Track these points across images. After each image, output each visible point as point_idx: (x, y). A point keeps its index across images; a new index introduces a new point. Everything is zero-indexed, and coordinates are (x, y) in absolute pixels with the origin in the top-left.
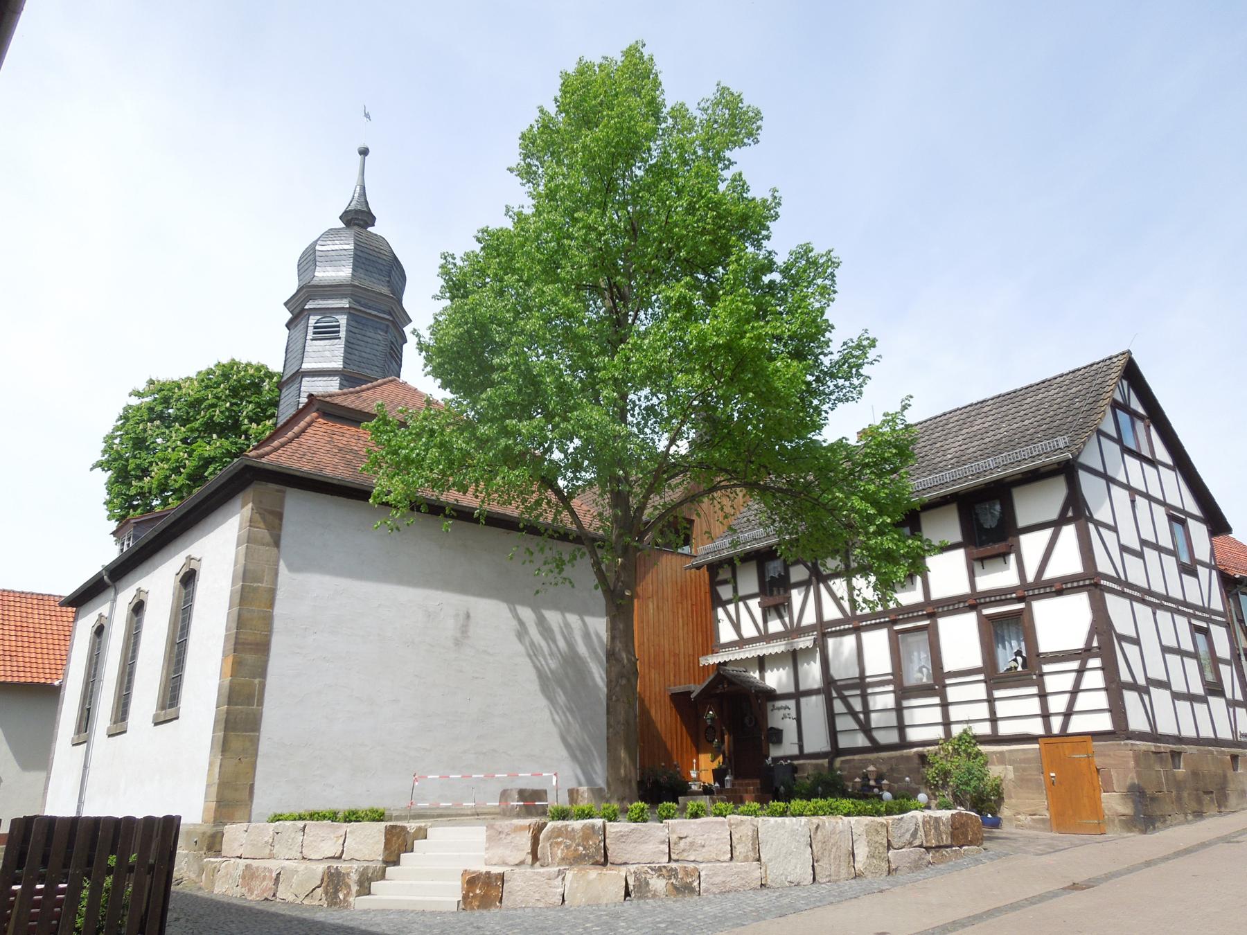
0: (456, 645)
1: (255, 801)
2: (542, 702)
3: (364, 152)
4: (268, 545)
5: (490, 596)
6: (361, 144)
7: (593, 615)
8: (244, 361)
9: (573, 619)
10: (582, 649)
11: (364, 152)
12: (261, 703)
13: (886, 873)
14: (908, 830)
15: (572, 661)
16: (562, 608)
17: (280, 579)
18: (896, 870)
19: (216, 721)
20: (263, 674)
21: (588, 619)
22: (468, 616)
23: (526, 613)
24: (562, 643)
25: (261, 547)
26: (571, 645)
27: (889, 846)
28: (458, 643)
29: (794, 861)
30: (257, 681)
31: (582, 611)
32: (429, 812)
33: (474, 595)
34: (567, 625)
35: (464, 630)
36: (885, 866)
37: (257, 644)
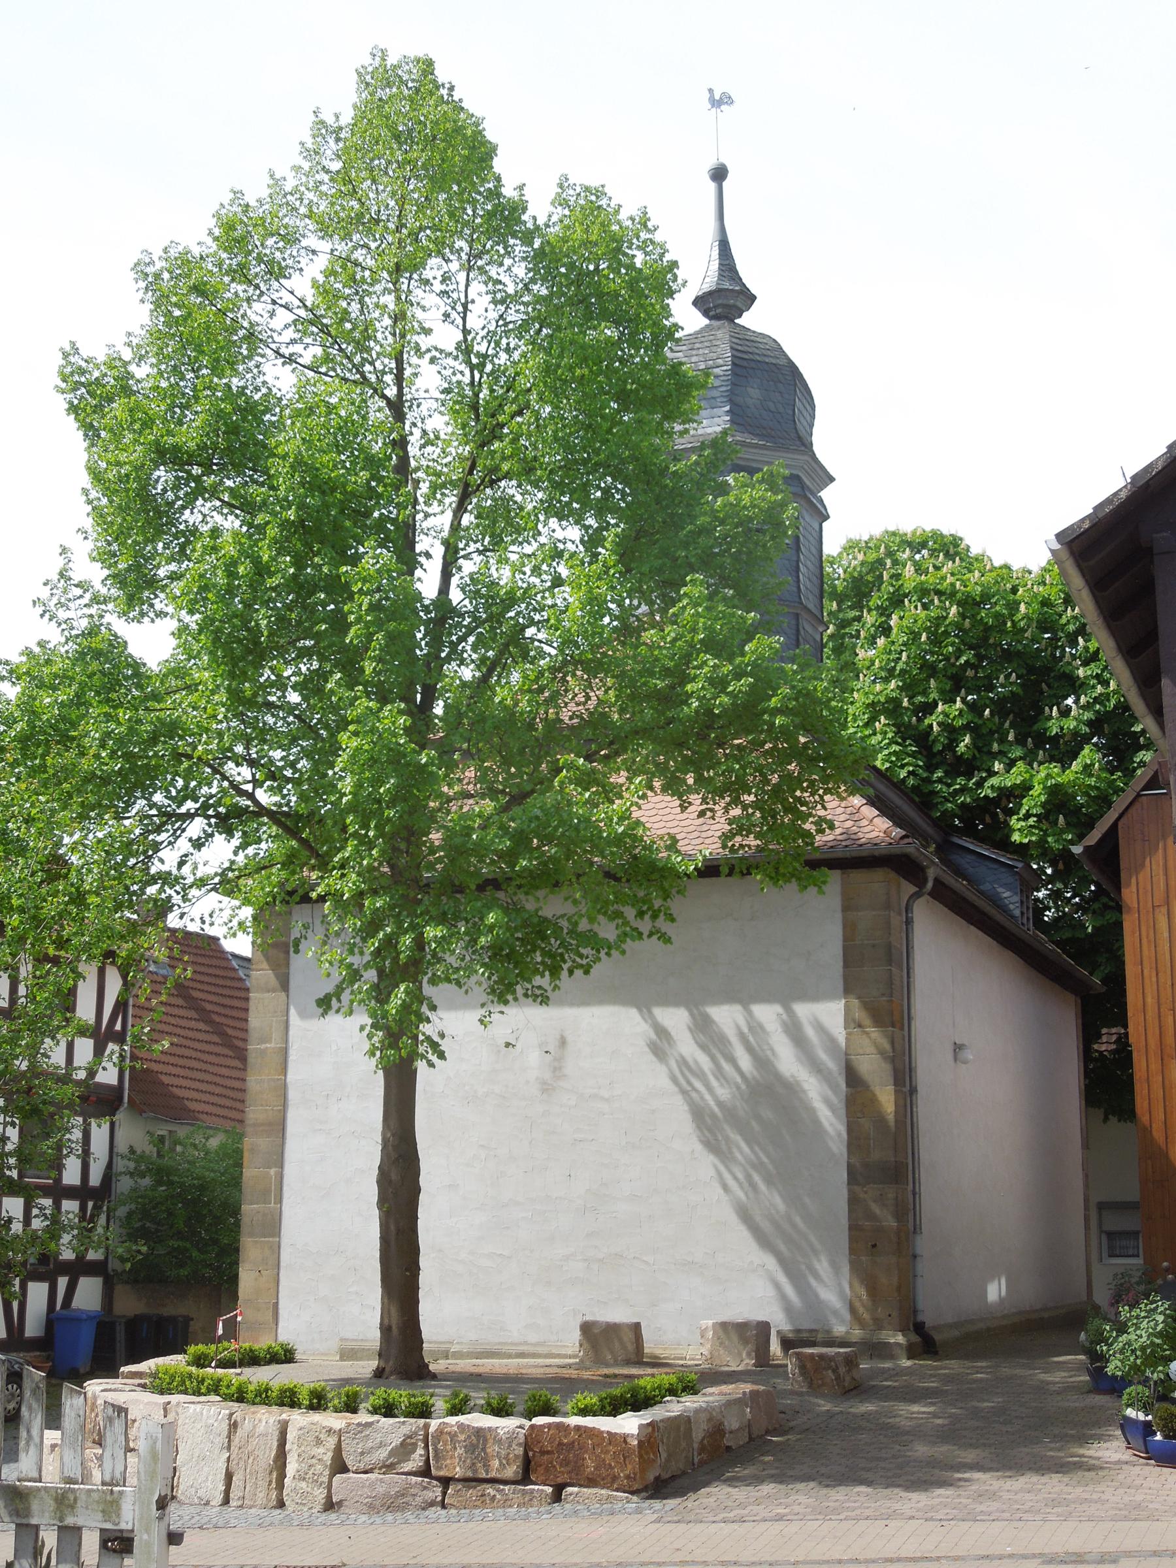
0: (544, 1091)
1: (281, 1324)
2: (706, 1165)
3: (719, 174)
4: (274, 990)
5: (601, 1002)
6: (711, 163)
7: (816, 997)
8: (866, 538)
9: (768, 1014)
10: (788, 1062)
11: (719, 174)
12: (280, 1200)
13: (319, 1507)
14: (381, 1445)
15: (769, 1095)
16: (741, 994)
17: (291, 1033)
18: (340, 1503)
19: (273, 1227)
20: (280, 1163)
21: (803, 1010)
22: (563, 1042)
23: (676, 1019)
24: (745, 1062)
25: (267, 995)
26: (763, 1062)
27: (340, 1466)
28: (546, 1088)
29: (206, 1469)
30: (272, 1171)
31: (788, 993)
32: (505, 1349)
33: (572, 1004)
34: (756, 1028)
35: (557, 1069)
36: (320, 1494)
37: (270, 1124)
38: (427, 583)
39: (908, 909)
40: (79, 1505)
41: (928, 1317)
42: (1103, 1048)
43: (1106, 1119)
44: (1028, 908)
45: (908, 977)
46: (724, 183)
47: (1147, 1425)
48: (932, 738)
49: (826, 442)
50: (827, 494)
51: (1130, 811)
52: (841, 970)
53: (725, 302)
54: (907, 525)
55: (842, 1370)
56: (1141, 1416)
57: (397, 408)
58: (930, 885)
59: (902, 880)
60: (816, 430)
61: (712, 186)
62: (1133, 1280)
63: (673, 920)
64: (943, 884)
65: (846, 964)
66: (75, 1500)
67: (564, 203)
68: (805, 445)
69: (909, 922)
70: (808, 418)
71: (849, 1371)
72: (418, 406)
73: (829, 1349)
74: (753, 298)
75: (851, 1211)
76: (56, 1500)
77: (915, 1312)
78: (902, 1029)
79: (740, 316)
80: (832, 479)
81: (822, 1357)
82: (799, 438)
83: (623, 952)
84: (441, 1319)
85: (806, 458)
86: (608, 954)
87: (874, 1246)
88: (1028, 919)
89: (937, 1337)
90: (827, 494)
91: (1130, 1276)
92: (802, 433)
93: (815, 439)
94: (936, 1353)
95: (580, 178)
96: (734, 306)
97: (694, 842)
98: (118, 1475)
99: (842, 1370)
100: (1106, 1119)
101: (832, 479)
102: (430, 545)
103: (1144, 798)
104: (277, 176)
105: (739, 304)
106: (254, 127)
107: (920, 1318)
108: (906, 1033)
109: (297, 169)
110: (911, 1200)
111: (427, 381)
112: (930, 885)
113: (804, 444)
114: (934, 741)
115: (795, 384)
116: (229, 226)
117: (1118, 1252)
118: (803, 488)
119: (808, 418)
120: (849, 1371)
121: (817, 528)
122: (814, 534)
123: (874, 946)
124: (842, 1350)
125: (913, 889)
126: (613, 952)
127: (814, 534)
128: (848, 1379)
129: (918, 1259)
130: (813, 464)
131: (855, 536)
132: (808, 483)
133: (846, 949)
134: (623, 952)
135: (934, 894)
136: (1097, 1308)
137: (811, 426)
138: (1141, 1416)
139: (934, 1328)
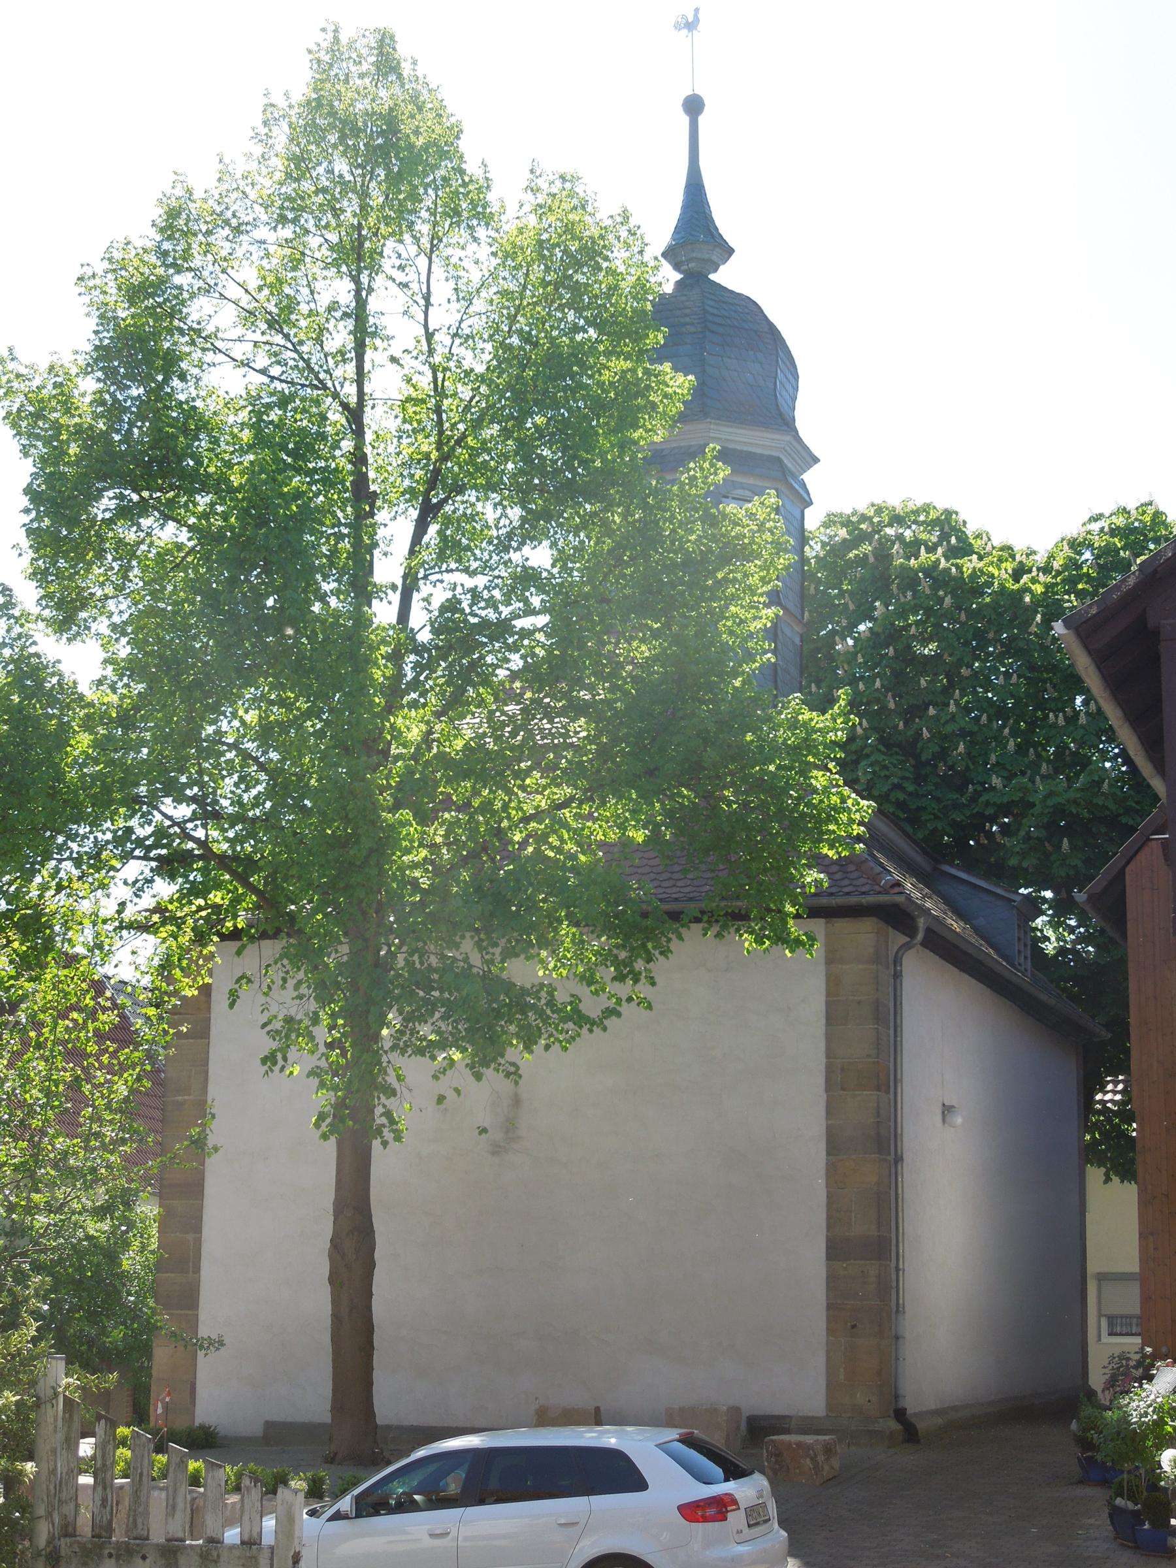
3: (694, 106)
11: (694, 106)
12: (197, 1269)
20: (197, 1228)
38: (384, 612)
39: (897, 961)
40: (222, 1559)
41: (912, 1404)
42: (1108, 1097)
43: (1108, 1179)
44: (1025, 945)
45: (896, 1036)
46: (701, 119)
47: (1135, 1514)
48: (919, 745)
49: (811, 417)
50: (809, 477)
51: (1138, 857)
52: (824, 1028)
53: (699, 255)
54: (895, 501)
55: (821, 1458)
56: (1130, 1505)
57: (355, 415)
58: (920, 936)
59: (890, 929)
60: (799, 404)
61: (686, 120)
62: (1132, 1363)
63: (653, 984)
64: (934, 932)
65: (830, 1020)
66: (218, 1556)
67: (535, 191)
68: (786, 423)
69: (897, 976)
70: (790, 389)
71: (827, 1460)
72: (373, 408)
73: (807, 1437)
74: (731, 251)
75: (829, 1288)
76: (201, 1556)
77: (897, 1397)
78: (888, 1093)
79: (716, 270)
80: (816, 460)
81: (800, 1445)
82: (781, 414)
83: (605, 1029)
84: (393, 1399)
85: (788, 438)
86: (591, 1031)
87: (854, 1327)
88: (1026, 958)
89: (921, 1425)
90: (809, 477)
91: (1128, 1359)
92: (784, 407)
93: (798, 414)
94: (918, 1442)
95: (552, 165)
96: (710, 260)
97: (665, 884)
98: (255, 1535)
99: (821, 1458)
100: (1108, 1179)
101: (816, 460)
102: (387, 569)
103: (1154, 843)
104: (226, 160)
105: (714, 258)
106: (208, 121)
107: (901, 1404)
108: (892, 1096)
109: (249, 156)
110: (894, 1277)
111: (385, 384)
112: (920, 936)
113: (787, 425)
114: (922, 750)
115: (778, 354)
116: (173, 214)
117: (1118, 1330)
118: (784, 472)
119: (790, 389)
120: (827, 1460)
121: (798, 516)
122: (796, 524)
123: (859, 1003)
124: (821, 1438)
125: (903, 939)
126: (595, 1028)
127: (796, 524)
128: (826, 1468)
129: (901, 1340)
130: (797, 445)
131: (836, 509)
132: (789, 465)
133: (829, 1005)
134: (605, 1029)
135: (924, 944)
136: (1091, 1394)
137: (794, 399)
138: (1130, 1505)
139: (915, 1414)
